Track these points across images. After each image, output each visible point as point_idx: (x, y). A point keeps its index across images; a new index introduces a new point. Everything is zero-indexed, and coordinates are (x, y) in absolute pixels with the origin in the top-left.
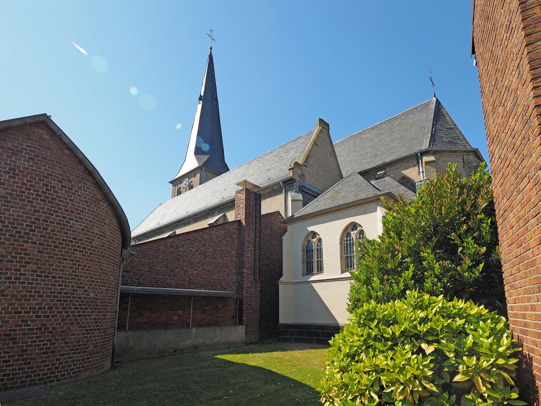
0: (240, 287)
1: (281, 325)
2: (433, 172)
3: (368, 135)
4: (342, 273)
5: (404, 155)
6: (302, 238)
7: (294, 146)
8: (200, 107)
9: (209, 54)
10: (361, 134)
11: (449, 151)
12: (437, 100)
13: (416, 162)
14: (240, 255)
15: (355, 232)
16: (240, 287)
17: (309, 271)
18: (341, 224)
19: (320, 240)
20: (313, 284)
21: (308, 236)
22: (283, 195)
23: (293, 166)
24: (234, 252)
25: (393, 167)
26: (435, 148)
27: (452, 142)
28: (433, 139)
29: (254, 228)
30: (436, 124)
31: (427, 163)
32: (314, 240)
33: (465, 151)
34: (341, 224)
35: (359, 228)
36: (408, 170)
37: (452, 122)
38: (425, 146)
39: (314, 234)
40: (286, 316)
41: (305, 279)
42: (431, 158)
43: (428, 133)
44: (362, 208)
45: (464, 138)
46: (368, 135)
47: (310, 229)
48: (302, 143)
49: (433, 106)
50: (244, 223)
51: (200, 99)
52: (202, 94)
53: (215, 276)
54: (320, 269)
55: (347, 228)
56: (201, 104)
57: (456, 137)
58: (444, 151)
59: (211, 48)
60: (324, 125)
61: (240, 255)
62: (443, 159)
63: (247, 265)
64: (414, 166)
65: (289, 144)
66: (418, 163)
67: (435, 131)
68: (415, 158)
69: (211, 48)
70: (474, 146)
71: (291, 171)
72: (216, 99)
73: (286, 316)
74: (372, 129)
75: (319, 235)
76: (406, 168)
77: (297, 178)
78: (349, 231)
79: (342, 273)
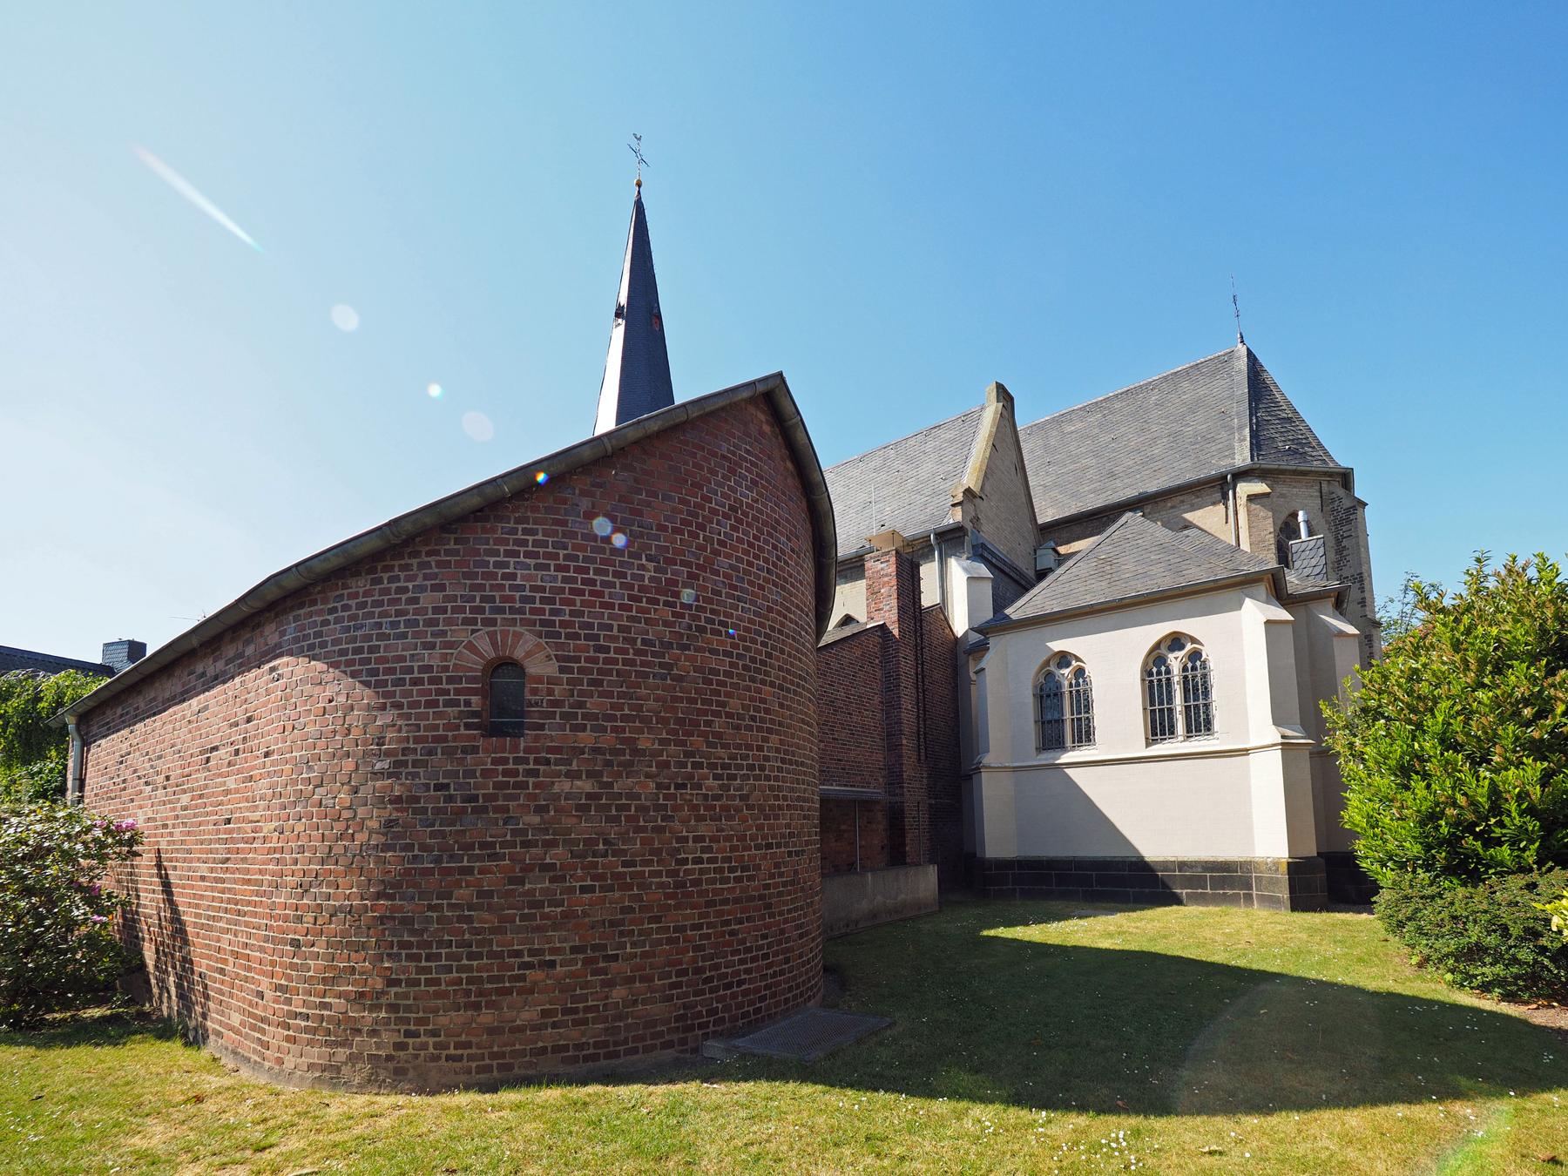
0: (894, 778)
1: (990, 861)
2: (1265, 518)
3: (1079, 425)
4: (1148, 745)
5: (1190, 476)
6: (1035, 667)
7: (929, 447)
8: (618, 334)
9: (634, 198)
10: (1058, 421)
11: (1295, 472)
12: (1249, 353)
13: (1218, 495)
14: (891, 705)
15: (1181, 654)
16: (894, 778)
17: (1051, 738)
18: (1150, 634)
19: (1080, 672)
20: (1069, 771)
21: (1047, 663)
22: (936, 564)
23: (960, 498)
24: (877, 699)
25: (1161, 505)
26: (1266, 464)
27: (1296, 452)
28: (1256, 444)
29: (912, 643)
30: (1257, 409)
31: (1252, 498)
32: (1066, 671)
33: (1325, 474)
34: (1150, 634)
35: (1189, 647)
36: (1199, 513)
37: (1289, 403)
38: (1242, 456)
39: (1064, 659)
40: (1000, 836)
41: (1046, 758)
42: (1260, 487)
43: (1241, 428)
44: (1202, 600)
45: (1319, 444)
46: (1079, 425)
47: (1057, 646)
48: (952, 441)
49: (1242, 364)
50: (896, 632)
51: (618, 315)
52: (623, 300)
53: (853, 754)
54: (1085, 735)
55: (1157, 646)
56: (621, 329)
57: (1304, 443)
58: (1283, 472)
59: (639, 185)
60: (1004, 395)
61: (891, 705)
62: (1284, 489)
63: (906, 731)
64: (1214, 504)
65: (912, 442)
66: (1225, 497)
67: (1257, 424)
68: (1220, 486)
69: (639, 185)
70: (1343, 462)
71: (959, 509)
72: (659, 317)
73: (1000, 836)
74: (1088, 410)
75: (1078, 659)
76: (1193, 508)
77: (969, 526)
78: (1163, 650)
79: (1148, 745)
